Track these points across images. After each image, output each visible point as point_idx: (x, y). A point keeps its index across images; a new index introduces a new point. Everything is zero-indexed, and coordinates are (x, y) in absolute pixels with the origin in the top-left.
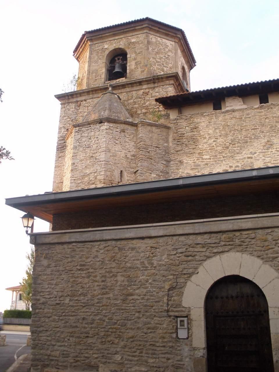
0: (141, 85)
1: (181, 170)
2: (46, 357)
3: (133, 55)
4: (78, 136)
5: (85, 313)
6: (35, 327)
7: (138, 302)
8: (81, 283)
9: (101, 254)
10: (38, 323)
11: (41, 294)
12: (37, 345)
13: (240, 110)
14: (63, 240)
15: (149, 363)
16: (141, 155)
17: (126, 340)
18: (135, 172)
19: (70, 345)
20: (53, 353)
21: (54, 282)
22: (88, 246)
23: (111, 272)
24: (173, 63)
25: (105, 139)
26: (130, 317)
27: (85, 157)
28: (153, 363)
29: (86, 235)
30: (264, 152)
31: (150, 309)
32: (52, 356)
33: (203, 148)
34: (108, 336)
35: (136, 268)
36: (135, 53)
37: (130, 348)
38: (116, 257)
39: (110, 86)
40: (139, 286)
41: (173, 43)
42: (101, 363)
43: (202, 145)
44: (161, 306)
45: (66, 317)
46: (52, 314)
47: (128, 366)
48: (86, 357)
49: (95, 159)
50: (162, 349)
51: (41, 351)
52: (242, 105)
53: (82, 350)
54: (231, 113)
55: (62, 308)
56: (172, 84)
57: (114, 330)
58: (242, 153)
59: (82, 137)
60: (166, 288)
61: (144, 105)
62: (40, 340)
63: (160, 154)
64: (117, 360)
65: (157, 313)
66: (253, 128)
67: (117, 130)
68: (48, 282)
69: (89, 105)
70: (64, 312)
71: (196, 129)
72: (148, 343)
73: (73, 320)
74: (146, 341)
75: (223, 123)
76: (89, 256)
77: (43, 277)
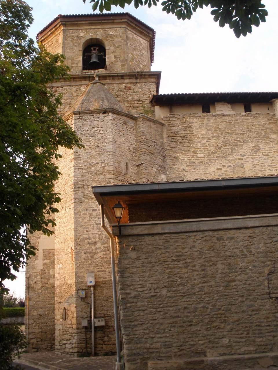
0: (123, 79)
1: (177, 166)
2: (145, 351)
3: (112, 48)
4: (79, 124)
5: (186, 303)
6: (128, 322)
7: (240, 287)
8: (178, 273)
9: (198, 244)
10: (131, 317)
11: (132, 287)
12: (132, 340)
13: (229, 115)
14: (155, 231)
15: (256, 342)
16: (144, 148)
17: (232, 324)
18: (138, 166)
19: (173, 336)
20: (153, 345)
21: (147, 274)
22: (183, 237)
23: (211, 261)
24: (146, 61)
25: (110, 130)
26: (233, 302)
27: (89, 146)
28: (261, 342)
29: (181, 226)
30: (253, 155)
31: (253, 292)
32: (153, 349)
33: (197, 147)
34: (213, 322)
35: (235, 256)
36: (114, 46)
37: (236, 331)
38: (214, 247)
39: (97, 76)
40: (240, 272)
41: (146, 42)
42: (209, 348)
43: (196, 144)
44: (263, 289)
45: (165, 309)
46: (147, 306)
47: (237, 347)
48: (191, 345)
49: (102, 149)
50: (268, 328)
51: (139, 346)
52: (231, 111)
53: (186, 338)
54: (221, 117)
55: (159, 299)
56: (154, 82)
57: (219, 315)
58: (233, 155)
59: (85, 125)
60: (265, 273)
61: (127, 99)
62: (134, 335)
63: (158, 149)
64: (225, 343)
65: (259, 296)
66: (241, 133)
67: (121, 122)
68: (138, 275)
69: (67, 92)
70: (162, 304)
71: (188, 128)
72: (254, 324)
73: (173, 310)
74: (252, 323)
75: (215, 126)
76: (186, 246)
77: (133, 269)
